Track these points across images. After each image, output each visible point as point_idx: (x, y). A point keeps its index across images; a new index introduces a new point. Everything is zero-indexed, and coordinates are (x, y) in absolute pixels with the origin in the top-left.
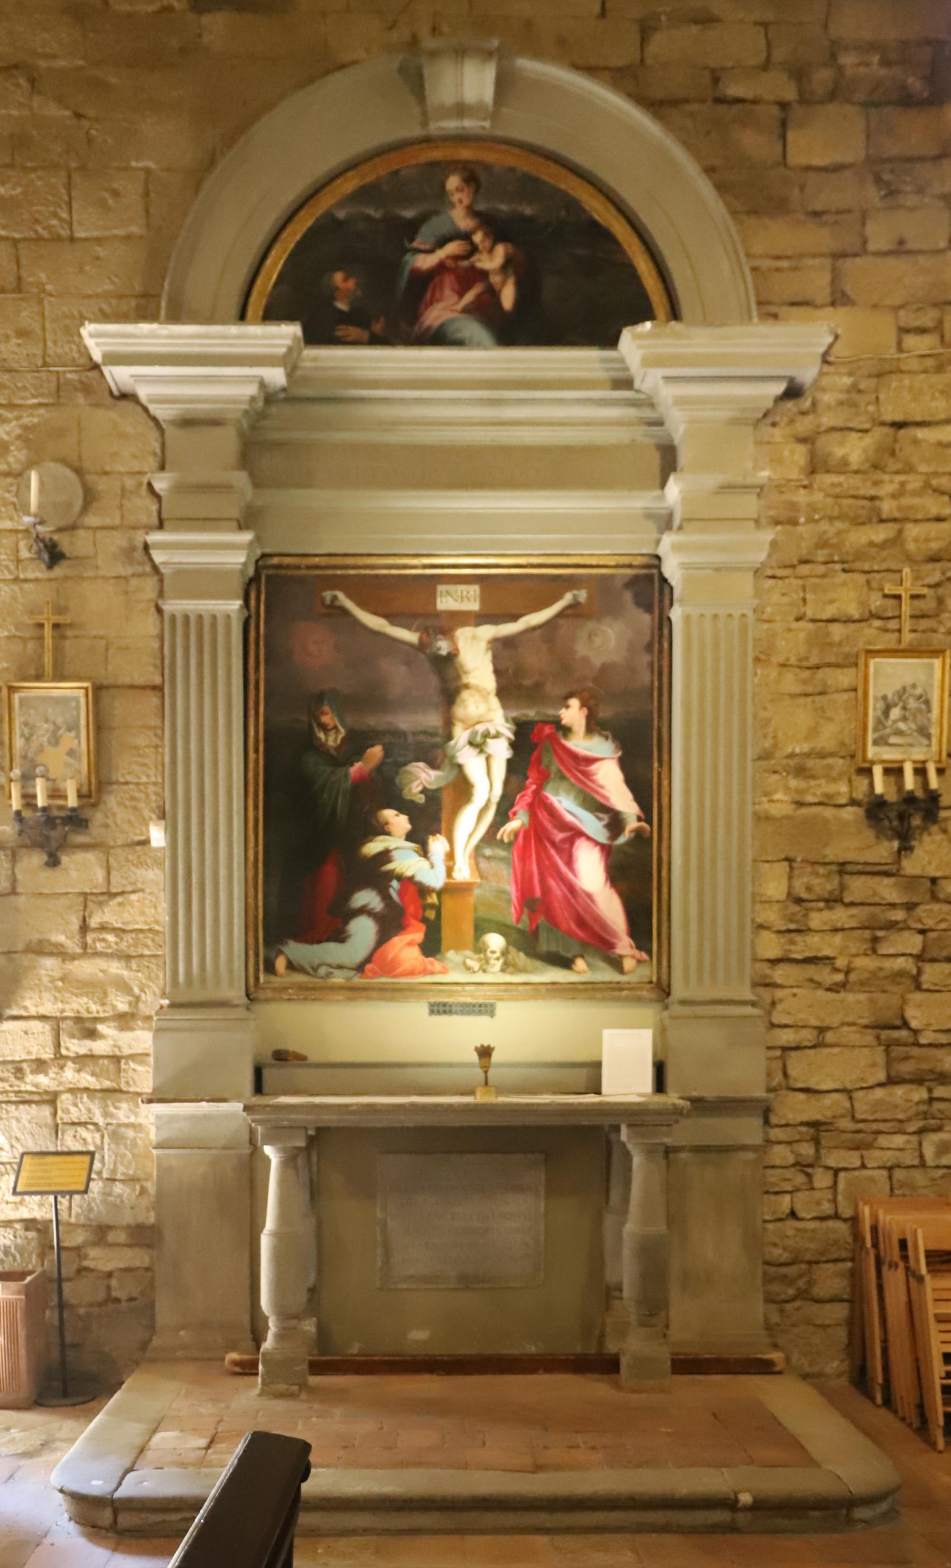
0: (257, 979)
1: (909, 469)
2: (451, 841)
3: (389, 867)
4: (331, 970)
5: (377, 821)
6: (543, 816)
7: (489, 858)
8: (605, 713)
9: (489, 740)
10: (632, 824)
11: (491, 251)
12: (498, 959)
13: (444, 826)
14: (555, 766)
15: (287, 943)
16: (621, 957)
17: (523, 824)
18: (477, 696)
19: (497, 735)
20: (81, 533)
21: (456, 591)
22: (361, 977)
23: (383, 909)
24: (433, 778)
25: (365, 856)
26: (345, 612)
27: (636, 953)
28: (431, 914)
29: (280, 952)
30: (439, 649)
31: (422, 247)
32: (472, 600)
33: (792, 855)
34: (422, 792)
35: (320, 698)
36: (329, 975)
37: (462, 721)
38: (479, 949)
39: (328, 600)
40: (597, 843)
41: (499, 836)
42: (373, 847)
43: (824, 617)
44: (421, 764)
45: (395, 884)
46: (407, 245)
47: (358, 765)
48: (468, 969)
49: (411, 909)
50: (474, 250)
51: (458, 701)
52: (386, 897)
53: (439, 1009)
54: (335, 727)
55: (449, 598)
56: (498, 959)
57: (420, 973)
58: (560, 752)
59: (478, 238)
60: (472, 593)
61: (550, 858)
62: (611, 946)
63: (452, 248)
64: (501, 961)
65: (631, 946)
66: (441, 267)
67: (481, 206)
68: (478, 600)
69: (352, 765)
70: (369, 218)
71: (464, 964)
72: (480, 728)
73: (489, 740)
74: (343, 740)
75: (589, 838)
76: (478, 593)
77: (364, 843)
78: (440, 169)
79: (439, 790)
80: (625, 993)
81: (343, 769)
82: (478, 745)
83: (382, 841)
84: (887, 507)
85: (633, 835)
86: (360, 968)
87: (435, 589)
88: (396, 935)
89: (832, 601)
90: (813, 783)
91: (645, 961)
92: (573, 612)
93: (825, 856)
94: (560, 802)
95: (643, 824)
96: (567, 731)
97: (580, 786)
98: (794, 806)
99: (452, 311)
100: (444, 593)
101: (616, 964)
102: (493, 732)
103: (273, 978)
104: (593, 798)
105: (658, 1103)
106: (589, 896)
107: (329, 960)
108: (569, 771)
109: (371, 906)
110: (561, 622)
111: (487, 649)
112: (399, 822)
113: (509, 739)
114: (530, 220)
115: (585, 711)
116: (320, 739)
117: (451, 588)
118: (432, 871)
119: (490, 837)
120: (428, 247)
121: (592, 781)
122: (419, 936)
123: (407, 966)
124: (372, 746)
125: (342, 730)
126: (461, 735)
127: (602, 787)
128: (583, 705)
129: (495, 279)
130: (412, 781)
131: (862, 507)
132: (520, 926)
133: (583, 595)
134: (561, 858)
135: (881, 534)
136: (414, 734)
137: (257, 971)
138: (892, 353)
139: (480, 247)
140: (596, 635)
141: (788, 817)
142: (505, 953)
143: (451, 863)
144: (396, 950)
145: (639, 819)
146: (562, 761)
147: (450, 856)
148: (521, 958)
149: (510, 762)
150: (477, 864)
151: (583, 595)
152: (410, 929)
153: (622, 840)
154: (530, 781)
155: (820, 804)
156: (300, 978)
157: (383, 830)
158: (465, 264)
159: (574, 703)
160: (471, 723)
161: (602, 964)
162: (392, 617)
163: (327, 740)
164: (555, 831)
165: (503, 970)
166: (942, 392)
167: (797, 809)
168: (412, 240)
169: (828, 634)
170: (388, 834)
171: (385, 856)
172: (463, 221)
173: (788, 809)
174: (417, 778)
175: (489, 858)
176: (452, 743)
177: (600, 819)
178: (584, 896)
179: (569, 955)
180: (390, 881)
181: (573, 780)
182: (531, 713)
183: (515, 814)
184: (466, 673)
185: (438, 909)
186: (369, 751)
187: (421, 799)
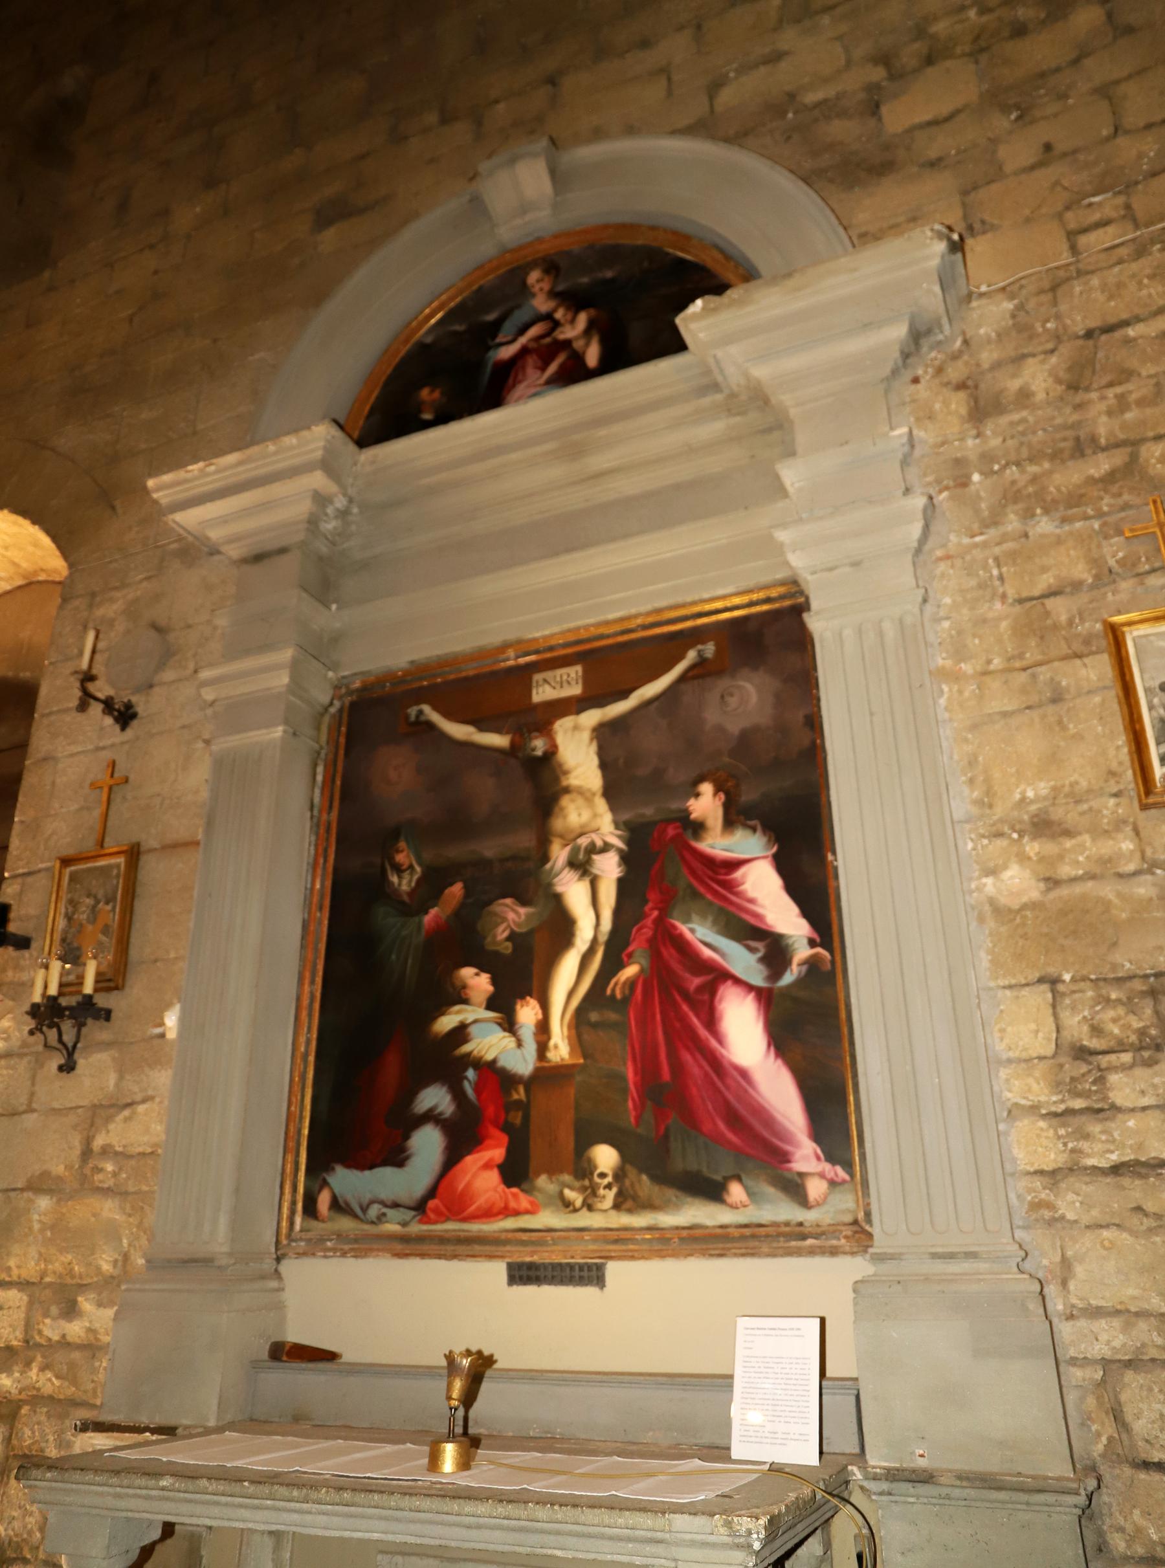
0: (291, 1223)
1: (1126, 375)
2: (545, 1006)
3: (466, 1048)
4: (385, 1210)
5: (453, 985)
6: (670, 955)
7: (595, 1026)
8: (749, 795)
9: (595, 857)
10: (802, 952)
11: (573, 321)
12: (609, 1187)
13: (535, 983)
14: (685, 879)
15: (333, 1169)
16: (801, 1175)
17: (642, 970)
18: (580, 801)
19: (606, 847)
20: (156, 690)
21: (555, 677)
22: (421, 1222)
23: (454, 1114)
24: (523, 917)
25: (437, 1035)
26: (431, 726)
27: (827, 1167)
28: (517, 1118)
29: (325, 1183)
30: (534, 749)
31: (504, 340)
32: (573, 683)
33: (1052, 970)
34: (508, 939)
35: (395, 834)
36: (381, 1218)
37: (561, 836)
38: (583, 1170)
39: (413, 718)
40: (750, 988)
41: (609, 992)
42: (446, 1023)
43: (1036, 592)
44: (508, 901)
45: (471, 1074)
46: (491, 343)
47: (434, 911)
48: (567, 1204)
49: (491, 1111)
50: (556, 324)
51: (556, 809)
52: (458, 1095)
53: (522, 1274)
54: (411, 867)
55: (547, 687)
56: (609, 1187)
57: (499, 1213)
58: (688, 856)
59: (559, 315)
60: (573, 675)
61: (683, 1019)
62: (784, 1157)
63: (533, 331)
64: (615, 1190)
65: (818, 1158)
66: (524, 351)
67: (560, 287)
68: (580, 681)
69: (426, 913)
70: (456, 333)
71: (561, 1195)
72: (583, 842)
73: (595, 857)
74: (418, 882)
75: (737, 981)
76: (580, 673)
77: (435, 1019)
78: (525, 269)
79: (530, 933)
80: (810, 1242)
81: (416, 919)
82: (581, 865)
83: (458, 1012)
84: (1104, 427)
85: (804, 968)
86: (420, 1207)
87: (530, 679)
88: (469, 1153)
89: (1044, 569)
90: (1069, 844)
91: (844, 1182)
92: (700, 672)
93: (1114, 967)
94: (692, 931)
95: (819, 950)
96: (698, 828)
97: (717, 902)
98: (1042, 885)
99: (536, 386)
100: (541, 682)
101: (794, 1189)
102: (599, 843)
103: (314, 1224)
104: (741, 920)
105: (484, 1223)
106: (744, 1073)
107: (384, 1195)
108: (702, 882)
109: (439, 1110)
110: (684, 687)
111: (592, 740)
112: (479, 983)
113: (620, 851)
114: (612, 281)
115: (722, 796)
116: (392, 884)
117: (548, 675)
118: (519, 1052)
119: (596, 997)
120: (509, 338)
121: (737, 894)
122: (497, 1154)
123: (481, 1202)
124: (451, 884)
125: (418, 869)
126: (559, 854)
127: (752, 901)
128: (718, 789)
129: (578, 345)
130: (497, 925)
131: (1065, 439)
132: (640, 1130)
133: (709, 649)
134: (698, 1016)
135: (1101, 465)
136: (503, 860)
137: (293, 1212)
138: (1066, 258)
139: (562, 321)
140: (732, 695)
141: (1034, 906)
142: (619, 1175)
143: (545, 1037)
144: (467, 1178)
145: (812, 943)
146: (693, 872)
147: (543, 1028)
148: (645, 1185)
149: (621, 882)
150: (579, 1036)
151: (709, 649)
152: (488, 1142)
153: (788, 978)
154: (650, 905)
155: (1092, 877)
156: (346, 1224)
157: (460, 997)
158: (548, 340)
159: (707, 788)
160: (572, 836)
161: (770, 1190)
162: (481, 724)
163: (400, 884)
164: (687, 975)
165: (617, 1206)
166: (1152, 277)
167: (1048, 890)
168: (494, 336)
169: (1047, 614)
170: (465, 1001)
171: (461, 1033)
172: (541, 304)
173: (1034, 892)
174: (504, 919)
175: (595, 1026)
176: (548, 866)
177: (752, 950)
178: (735, 1073)
179: (718, 1177)
180: (465, 1070)
181: (709, 897)
182: (649, 812)
183: (630, 956)
184: (566, 773)
185: (525, 1107)
186: (447, 891)
187: (507, 949)
